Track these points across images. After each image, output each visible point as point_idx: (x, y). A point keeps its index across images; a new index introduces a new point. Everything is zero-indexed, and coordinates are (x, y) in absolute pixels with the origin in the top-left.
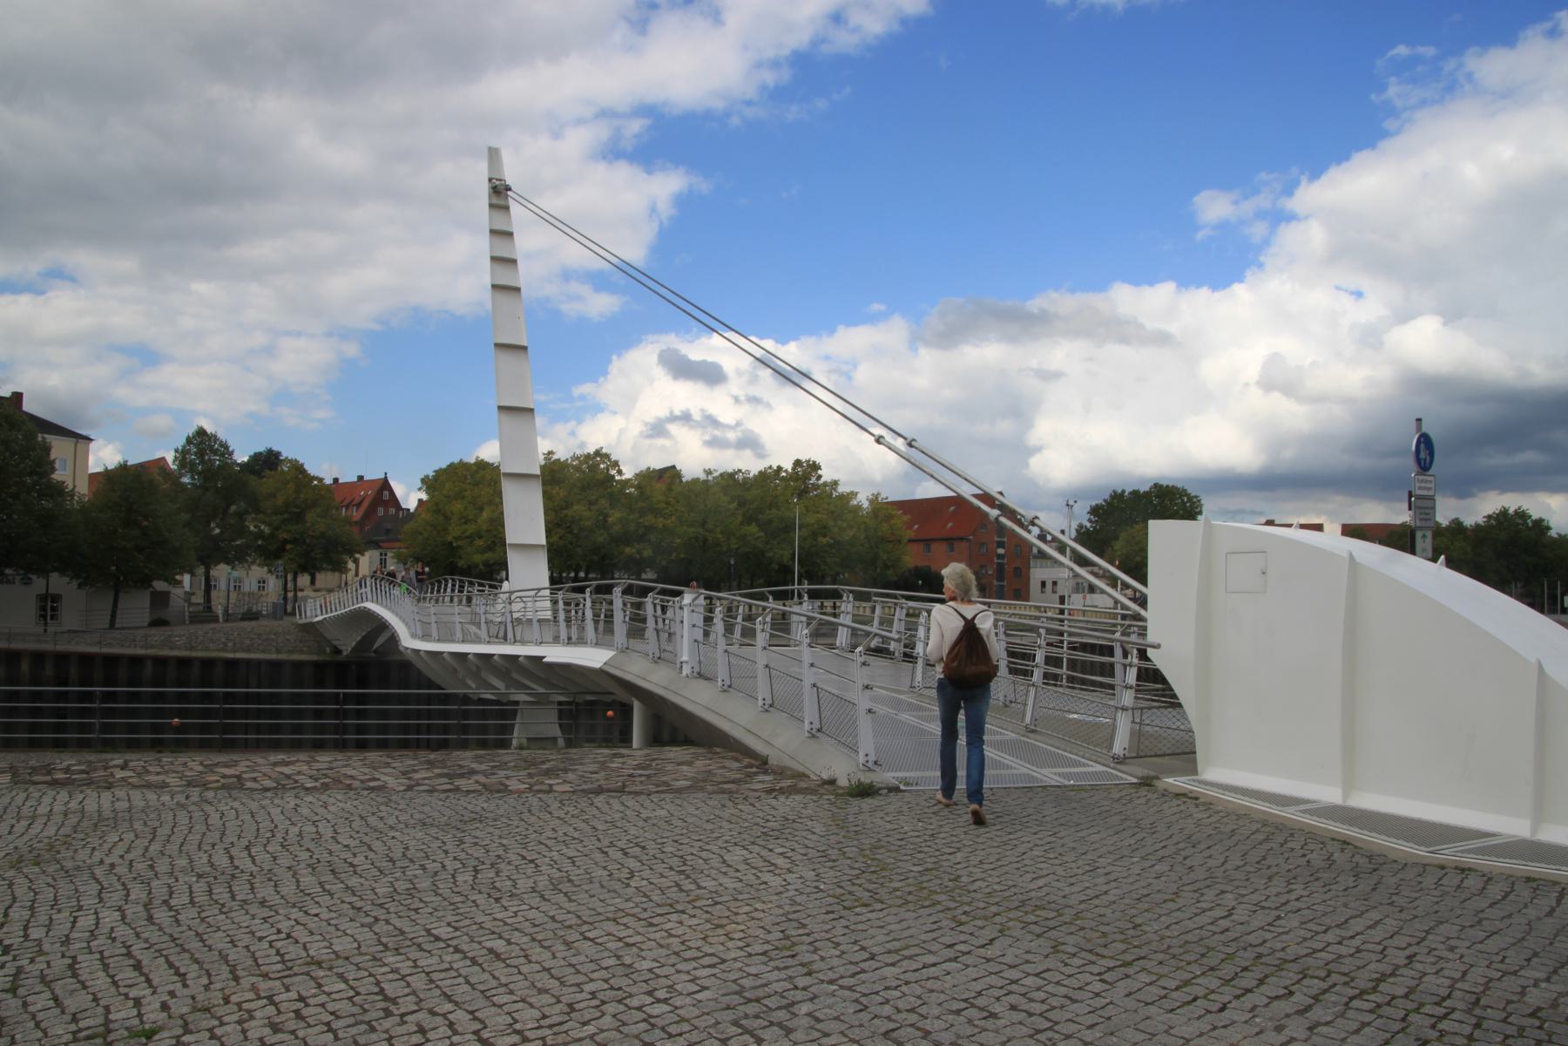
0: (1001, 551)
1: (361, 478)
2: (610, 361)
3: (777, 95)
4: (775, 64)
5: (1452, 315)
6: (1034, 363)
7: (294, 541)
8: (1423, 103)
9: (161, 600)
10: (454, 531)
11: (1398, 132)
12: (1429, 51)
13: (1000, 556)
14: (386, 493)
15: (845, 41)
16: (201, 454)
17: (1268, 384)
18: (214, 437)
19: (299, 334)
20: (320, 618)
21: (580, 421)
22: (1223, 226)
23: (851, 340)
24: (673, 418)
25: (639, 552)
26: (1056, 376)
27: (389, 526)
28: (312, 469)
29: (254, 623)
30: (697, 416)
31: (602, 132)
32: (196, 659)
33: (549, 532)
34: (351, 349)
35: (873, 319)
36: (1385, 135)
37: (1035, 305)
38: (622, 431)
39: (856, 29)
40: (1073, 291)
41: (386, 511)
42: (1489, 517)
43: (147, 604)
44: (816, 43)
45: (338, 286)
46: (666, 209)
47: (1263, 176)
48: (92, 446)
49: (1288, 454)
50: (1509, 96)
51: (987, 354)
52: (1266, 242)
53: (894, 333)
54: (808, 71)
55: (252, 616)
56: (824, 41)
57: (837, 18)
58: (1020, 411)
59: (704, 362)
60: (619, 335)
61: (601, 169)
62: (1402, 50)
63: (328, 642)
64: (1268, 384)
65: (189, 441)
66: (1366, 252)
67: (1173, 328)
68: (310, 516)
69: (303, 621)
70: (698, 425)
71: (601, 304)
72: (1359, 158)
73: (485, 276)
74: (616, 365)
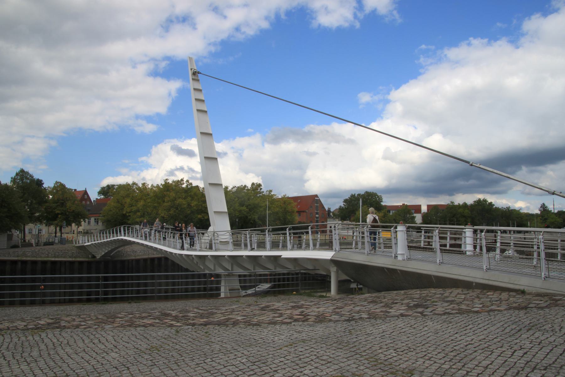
0: (317, 216)
2: (152, 148)
3: (214, 55)
4: (215, 44)
5: (446, 134)
6: (306, 150)
7: (62, 214)
8: (431, 64)
9: (10, 237)
10: (126, 210)
11: (424, 73)
12: (433, 47)
13: (317, 218)
14: (86, 196)
15: (240, 37)
16: (22, 179)
17: (385, 158)
18: (28, 173)
19: (33, 137)
20: (89, 243)
21: (142, 171)
22: (368, 104)
23: (241, 142)
24: (177, 169)
25: (203, 217)
26: (313, 154)
27: (89, 208)
28: (68, 186)
29: (51, 246)
30: (186, 168)
31: (152, 66)
32: (39, 261)
33: (228, 209)
34: (54, 143)
35: (249, 135)
36: (420, 74)
37: (306, 129)
38: (158, 174)
39: (244, 33)
40: (318, 124)
41: (86, 202)
42: (475, 202)
43: (6, 239)
44: (230, 37)
45: (50, 119)
46: (174, 94)
47: (381, 88)
49: (394, 181)
50: (457, 63)
51: (289, 146)
52: (383, 110)
53: (256, 139)
54: (227, 47)
55: (52, 244)
56: (233, 36)
57: (237, 29)
58: (302, 167)
59: (188, 150)
60: (156, 139)
61: (150, 80)
62: (423, 46)
63: (90, 253)
64: (385, 158)
65: (17, 174)
66: (413, 113)
67: (352, 138)
68: (69, 204)
69: (77, 245)
70: (186, 172)
71: (150, 128)
72: (412, 82)
74: (154, 150)
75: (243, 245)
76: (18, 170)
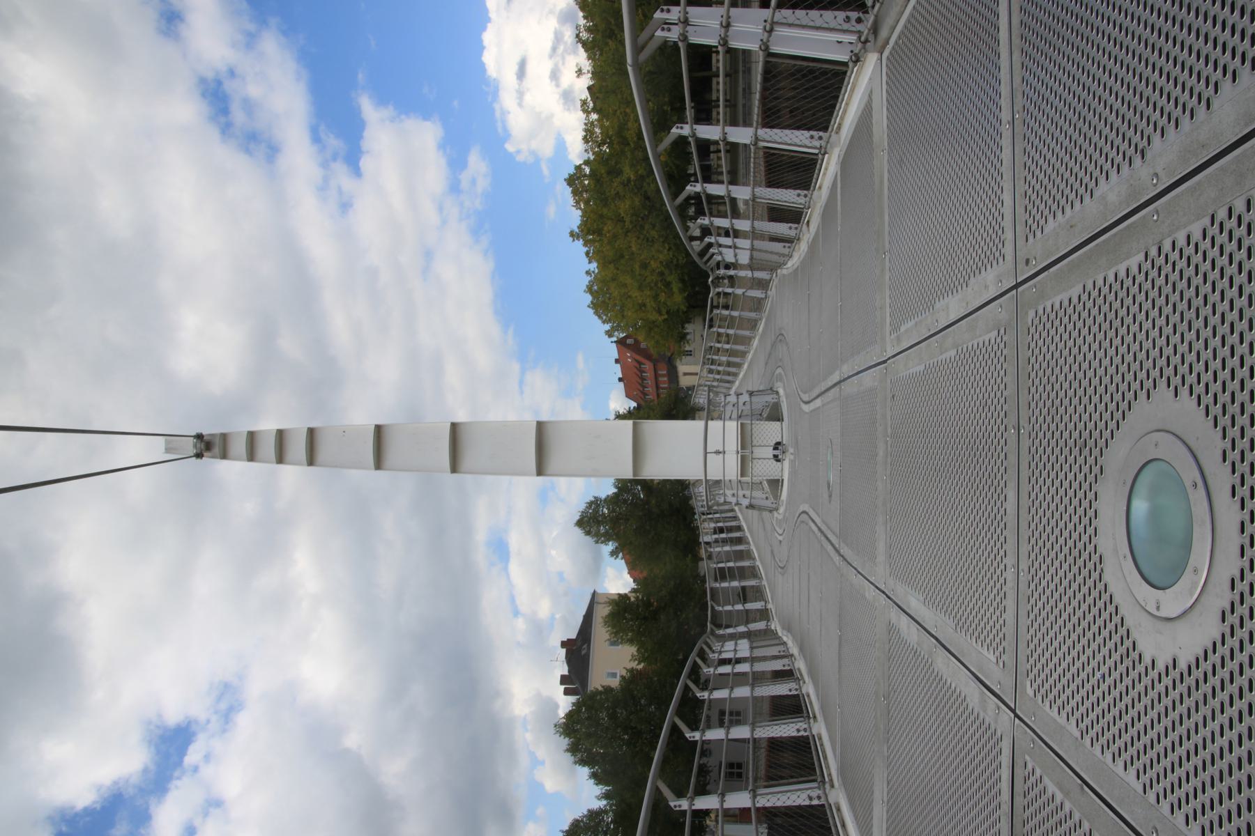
1: (617, 361)
46: (388, 112)
48: (599, 591)
61: (366, 163)
65: (588, 533)
73: (292, 475)
75: (787, 729)
76: (578, 532)
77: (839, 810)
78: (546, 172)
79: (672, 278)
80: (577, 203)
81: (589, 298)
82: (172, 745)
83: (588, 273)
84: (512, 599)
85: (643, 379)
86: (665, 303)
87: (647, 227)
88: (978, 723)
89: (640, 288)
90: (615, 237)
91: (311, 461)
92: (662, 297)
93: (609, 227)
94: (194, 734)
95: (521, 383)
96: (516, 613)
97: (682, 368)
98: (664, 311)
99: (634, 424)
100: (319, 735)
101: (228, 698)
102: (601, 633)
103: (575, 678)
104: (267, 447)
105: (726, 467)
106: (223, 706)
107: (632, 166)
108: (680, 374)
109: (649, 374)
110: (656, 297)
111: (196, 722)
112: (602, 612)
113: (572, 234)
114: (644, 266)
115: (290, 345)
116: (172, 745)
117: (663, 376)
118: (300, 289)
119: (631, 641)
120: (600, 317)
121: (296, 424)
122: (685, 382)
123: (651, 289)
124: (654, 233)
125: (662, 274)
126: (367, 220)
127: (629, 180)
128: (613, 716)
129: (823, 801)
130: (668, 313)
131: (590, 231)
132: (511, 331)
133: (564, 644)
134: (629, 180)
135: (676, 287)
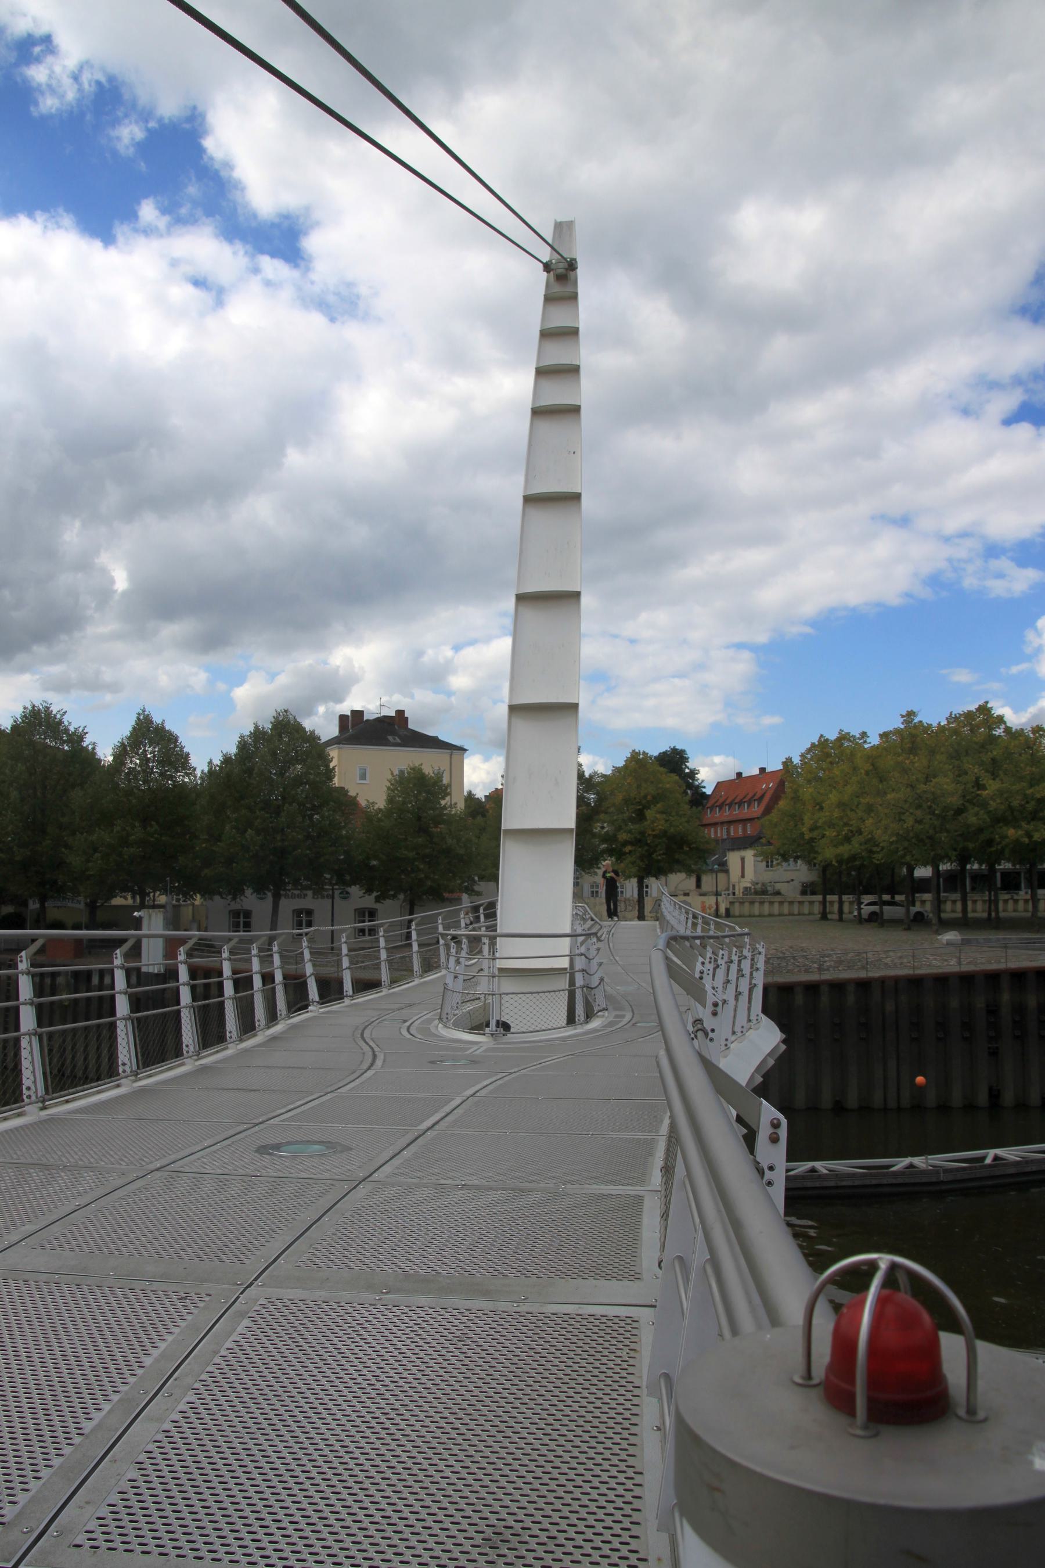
1: (762, 770)
61: (1024, 431)
77: (19, 1115)
78: (1015, 670)
79: (855, 846)
80: (956, 719)
81: (832, 736)
82: (281, 239)
83: (864, 734)
84: (472, 642)
85: (740, 804)
86: (823, 836)
87: (919, 813)
88: (258, 1245)
89: (841, 805)
90: (905, 771)
91: (537, 412)
92: (830, 833)
93: (919, 762)
94: (296, 266)
95: (740, 646)
96: (457, 648)
97: (749, 854)
98: (815, 834)
99: (572, 830)
100: (302, 415)
101: (341, 304)
102: (400, 760)
103: (359, 729)
104: (558, 354)
105: (513, 953)
106: (331, 299)
107: (1001, 792)
108: (743, 853)
109: (746, 812)
110: (831, 825)
111: (308, 269)
112: (429, 762)
113: (911, 714)
114: (870, 809)
115: (781, 351)
116: (281, 239)
117: (745, 830)
118: (846, 363)
119: (390, 800)
120: (809, 750)
121: (588, 392)
122: (733, 859)
123: (841, 818)
124: (910, 822)
125: (860, 832)
126: (949, 439)
127: (983, 787)
128: (298, 781)
129: (26, 1100)
130: (812, 840)
131: (912, 738)
132: (808, 630)
133: (400, 713)
134: (983, 787)
135: (845, 850)
